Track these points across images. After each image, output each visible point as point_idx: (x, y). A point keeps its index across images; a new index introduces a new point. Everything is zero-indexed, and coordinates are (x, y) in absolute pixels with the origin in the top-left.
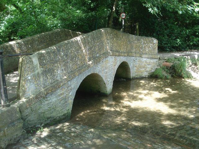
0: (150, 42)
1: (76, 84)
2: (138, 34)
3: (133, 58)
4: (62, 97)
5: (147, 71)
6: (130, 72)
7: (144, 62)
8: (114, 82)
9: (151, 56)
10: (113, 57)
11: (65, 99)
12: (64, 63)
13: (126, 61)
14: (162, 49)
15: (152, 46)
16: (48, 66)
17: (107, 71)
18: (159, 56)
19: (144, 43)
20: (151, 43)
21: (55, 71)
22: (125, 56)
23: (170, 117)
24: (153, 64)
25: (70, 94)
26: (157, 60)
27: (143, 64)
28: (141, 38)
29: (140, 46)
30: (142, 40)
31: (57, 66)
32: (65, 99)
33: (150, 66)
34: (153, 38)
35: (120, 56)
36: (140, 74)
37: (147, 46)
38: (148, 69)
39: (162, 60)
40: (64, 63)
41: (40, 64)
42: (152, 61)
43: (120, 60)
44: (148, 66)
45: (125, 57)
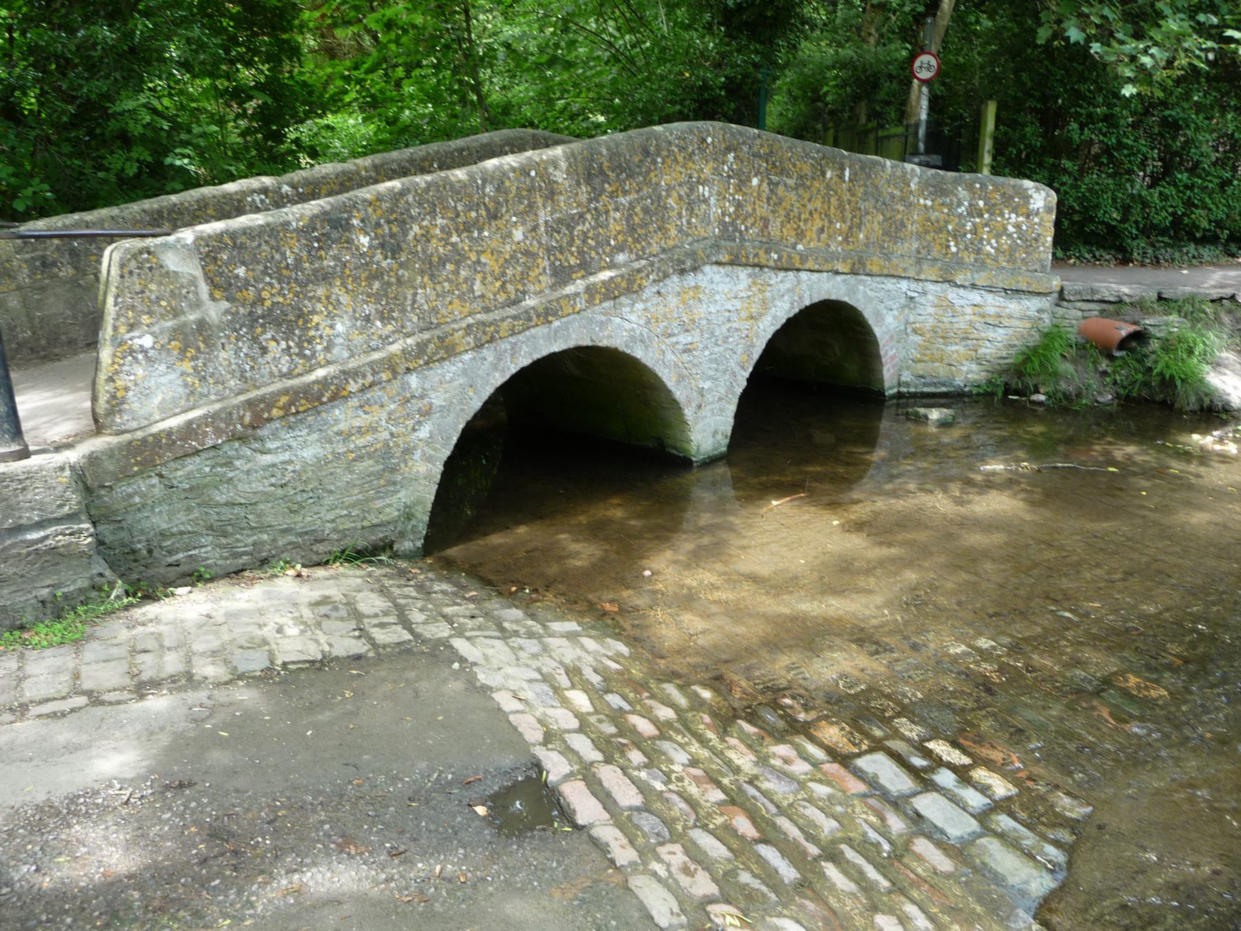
0: (1007, 199)
1: (462, 387)
2: (831, 140)
3: (904, 285)
4: (361, 442)
5: (978, 360)
6: (879, 357)
7: (969, 310)
8: (746, 401)
9: (1002, 281)
10: (743, 273)
11: (388, 462)
12: (376, 285)
13: (846, 299)
14: (1079, 235)
15: (1018, 226)
16: (265, 294)
17: (698, 342)
18: (1056, 283)
19: (974, 211)
20: (1015, 210)
21: (316, 319)
22: (837, 273)
23: (806, 898)
24: (1017, 323)
25: (424, 433)
26: (1045, 303)
27: (961, 323)
28: (956, 182)
29: (947, 222)
30: (962, 192)
31: (328, 298)
32: (388, 462)
33: (1000, 334)
34: (1027, 183)
35: (798, 270)
36: (942, 371)
37: (987, 225)
38: (987, 350)
39: (1079, 304)
40: (376, 285)
41: (210, 280)
42: (1014, 306)
43: (786, 296)
44: (991, 334)
45: (839, 278)
